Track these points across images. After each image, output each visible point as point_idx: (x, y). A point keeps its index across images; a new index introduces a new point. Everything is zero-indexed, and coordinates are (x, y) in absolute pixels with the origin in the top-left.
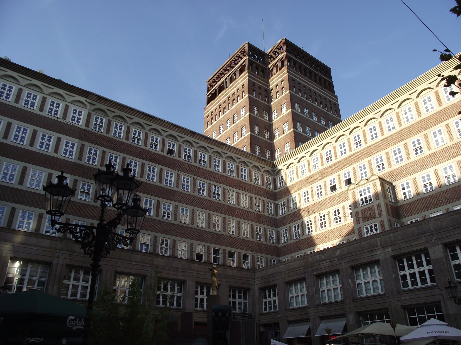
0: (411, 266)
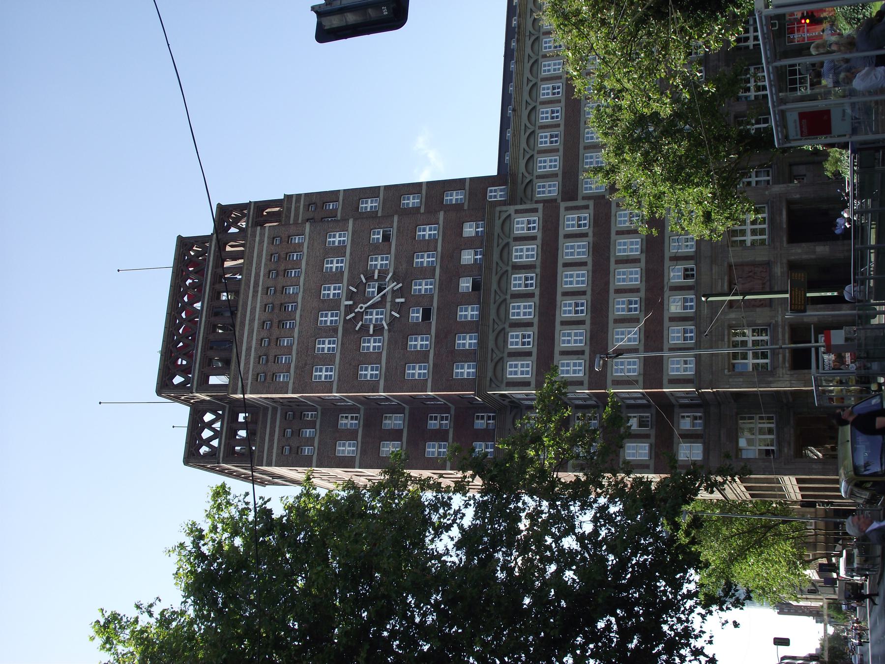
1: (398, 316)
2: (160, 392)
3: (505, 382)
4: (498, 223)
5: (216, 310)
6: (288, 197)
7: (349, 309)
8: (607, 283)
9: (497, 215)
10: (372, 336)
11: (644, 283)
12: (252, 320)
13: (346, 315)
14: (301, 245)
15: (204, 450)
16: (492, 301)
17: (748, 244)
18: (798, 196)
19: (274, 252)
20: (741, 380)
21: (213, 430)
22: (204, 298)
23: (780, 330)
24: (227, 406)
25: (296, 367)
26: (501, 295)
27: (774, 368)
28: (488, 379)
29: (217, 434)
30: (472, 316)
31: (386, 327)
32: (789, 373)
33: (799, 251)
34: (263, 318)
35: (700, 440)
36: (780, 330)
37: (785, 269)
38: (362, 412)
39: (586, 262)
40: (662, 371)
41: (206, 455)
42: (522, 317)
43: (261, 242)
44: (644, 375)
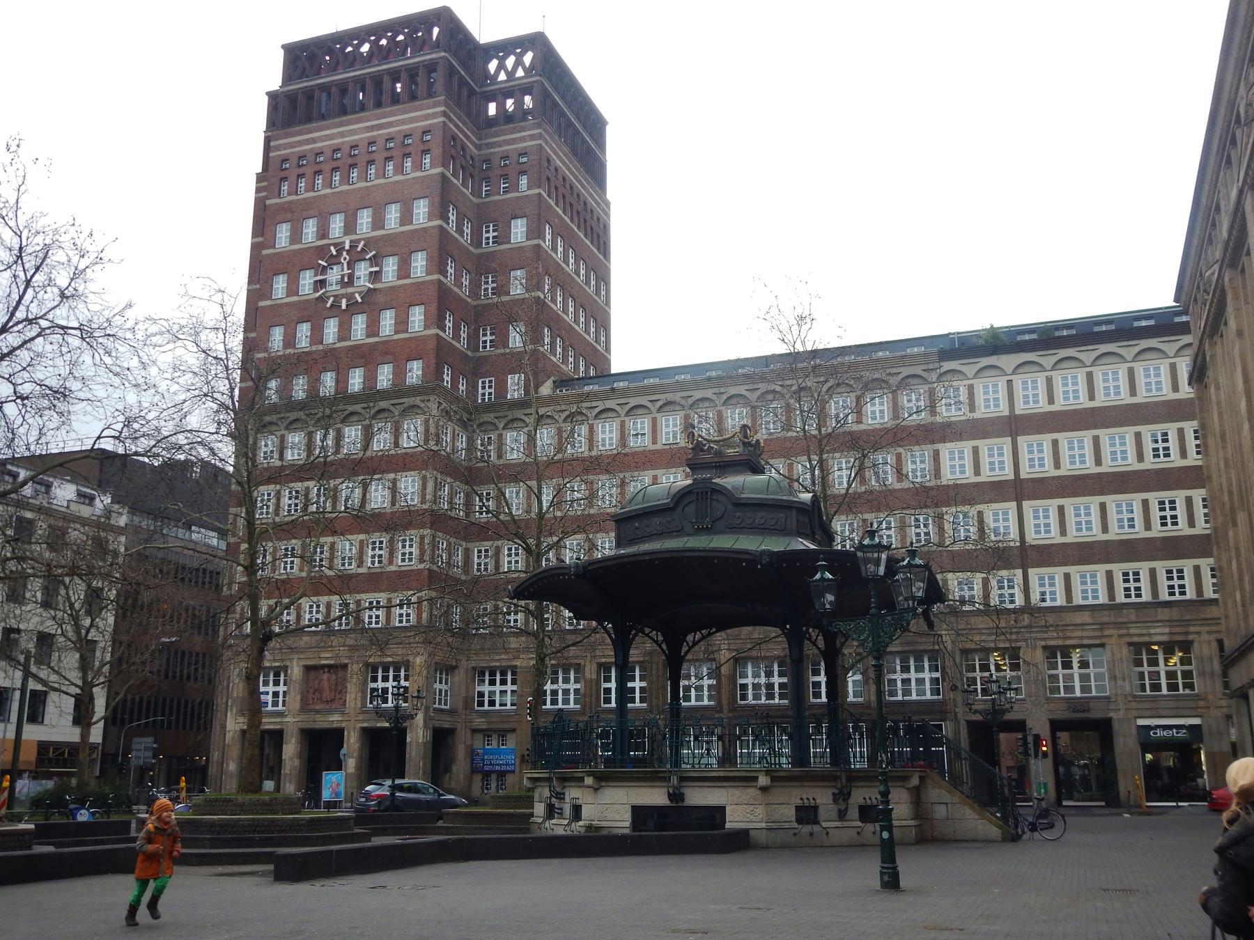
0: (492, 683)
17: (285, 688)
22: (531, 76)
23: (278, 720)
33: (352, 741)
36: (278, 720)
37: (335, 726)
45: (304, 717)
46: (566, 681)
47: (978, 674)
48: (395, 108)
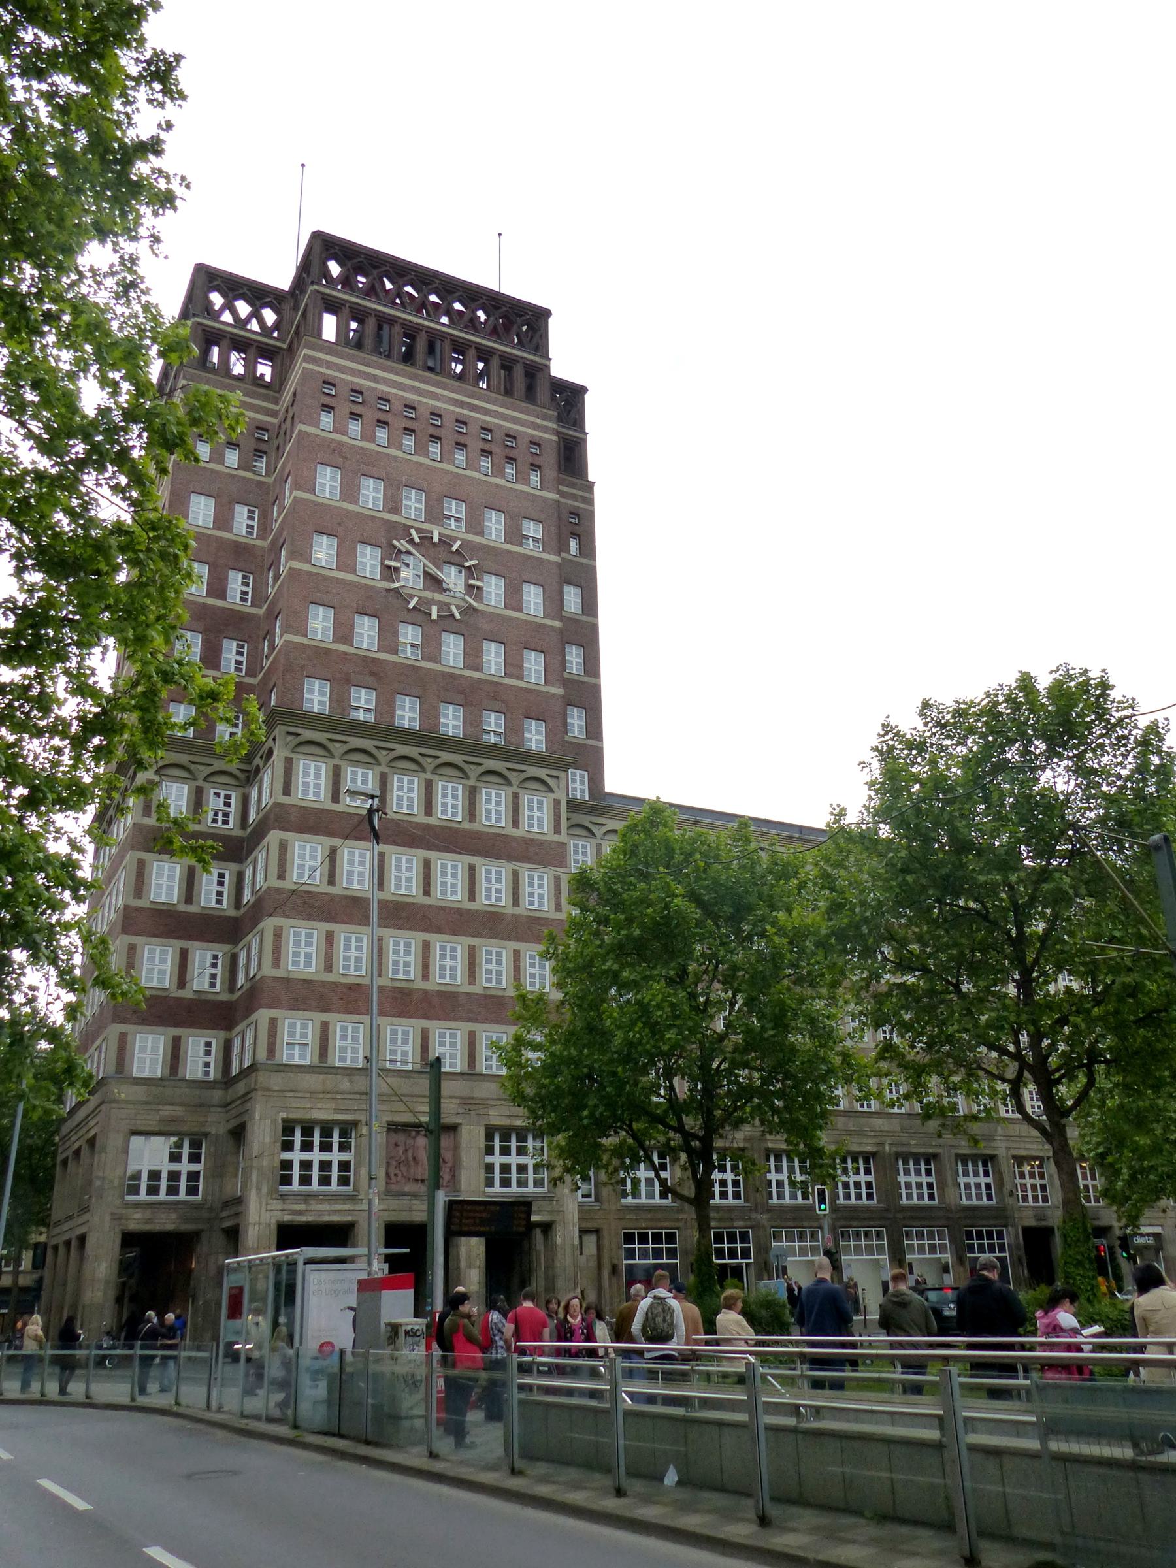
0: (307, 1147)
1: (411, 606)
2: (317, 236)
3: (292, 755)
4: (542, 773)
5: (434, 340)
6: (590, 487)
7: (426, 537)
8: (439, 931)
9: (554, 773)
10: (382, 563)
11: (437, 988)
12: (418, 391)
13: (418, 530)
14: (527, 481)
15: (217, 299)
16: (424, 751)
18: (559, 1241)
19: (519, 442)
20: (267, 1140)
21: (248, 320)
23: (347, 1207)
24: (285, 346)
25: (340, 443)
26: (433, 766)
27: (283, 1197)
28: (299, 731)
29: (241, 323)
30: (403, 717)
31: (394, 586)
32: (274, 1221)
34: (421, 409)
35: (167, 1071)
36: (347, 1207)
38: (258, 543)
39: (474, 900)
40: (292, 1008)
41: (209, 304)
42: (395, 794)
43: (535, 426)
44: (288, 980)
45: (394, 1203)
46: (505, 1151)
47: (1028, 1181)
48: (401, 366)
